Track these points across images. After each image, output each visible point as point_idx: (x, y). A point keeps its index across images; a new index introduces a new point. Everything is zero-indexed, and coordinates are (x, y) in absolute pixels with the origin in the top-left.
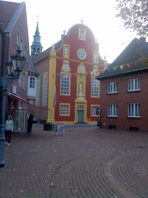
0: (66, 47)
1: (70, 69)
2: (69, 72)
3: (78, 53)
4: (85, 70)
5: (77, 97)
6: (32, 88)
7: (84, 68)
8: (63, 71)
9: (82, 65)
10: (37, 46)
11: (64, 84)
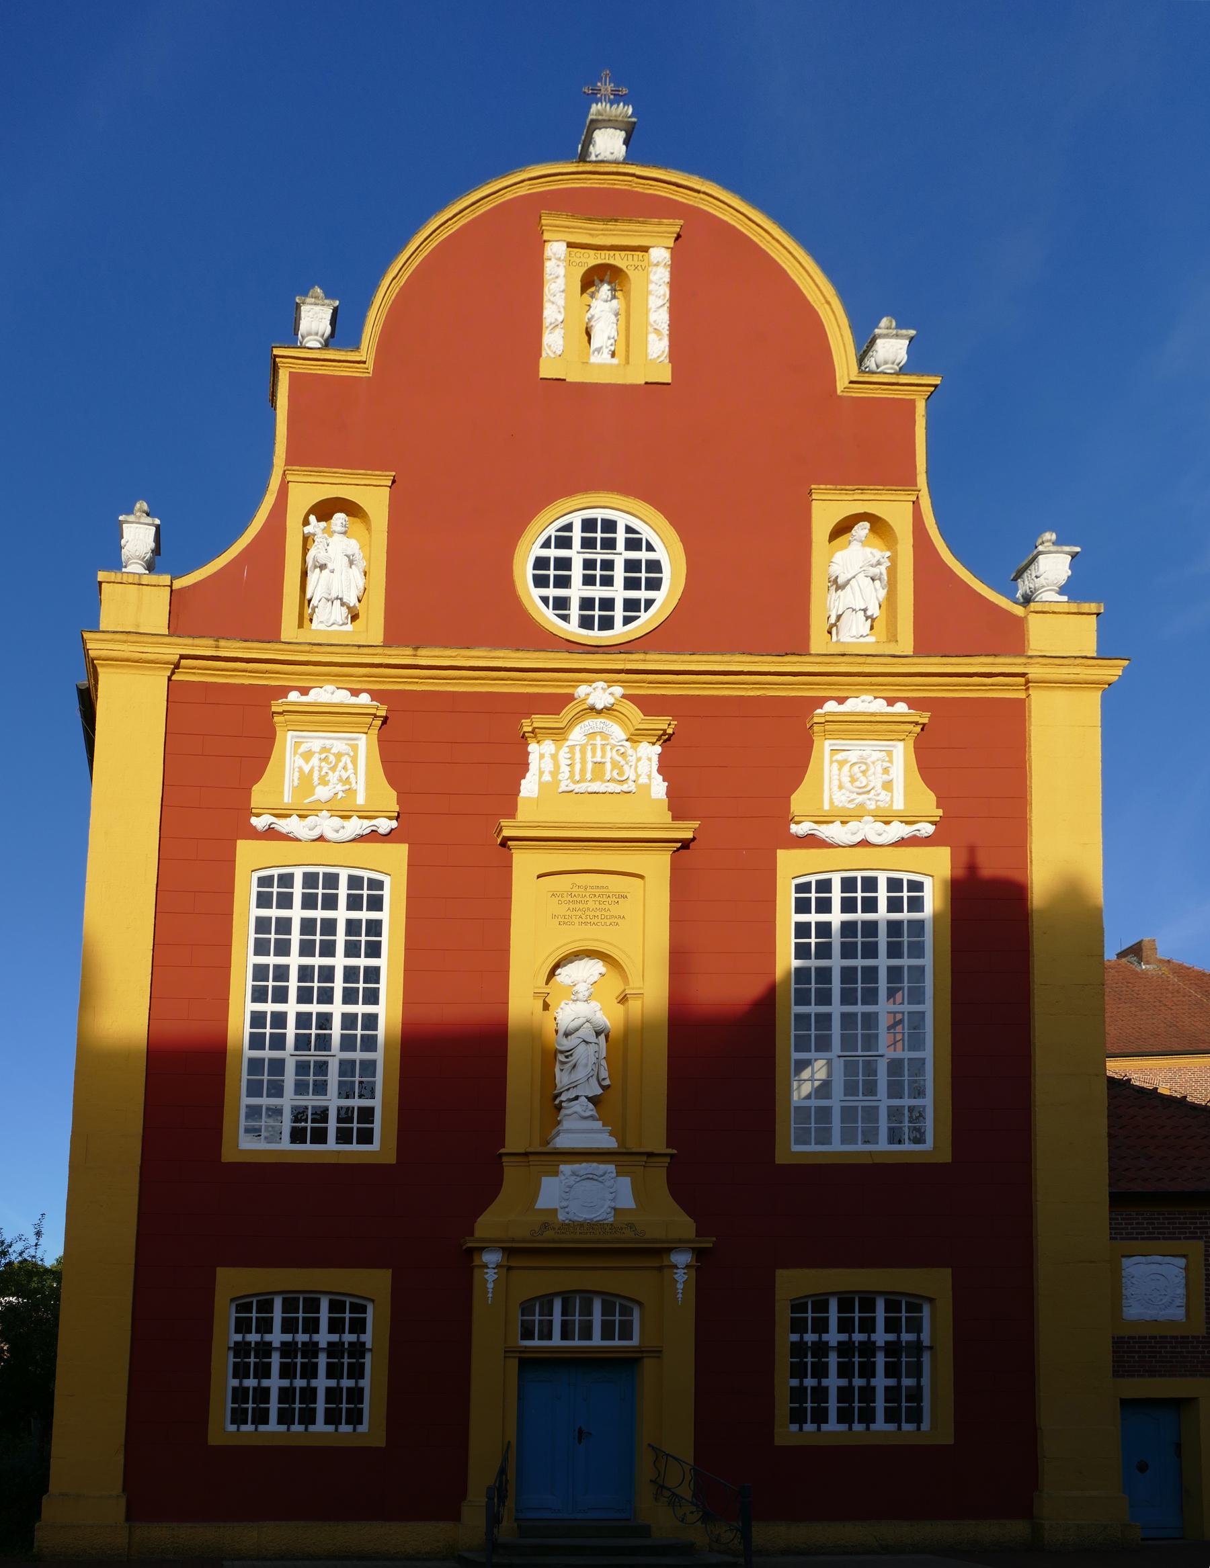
0: (324, 510)
1: (389, 799)
2: (373, 836)
3: (525, 572)
4: (659, 788)
5: (512, 1174)
6: (321, 870)
7: (650, 752)
8: (271, 834)
9: (607, 711)
10: (693, 1255)
11: (322, 1383)
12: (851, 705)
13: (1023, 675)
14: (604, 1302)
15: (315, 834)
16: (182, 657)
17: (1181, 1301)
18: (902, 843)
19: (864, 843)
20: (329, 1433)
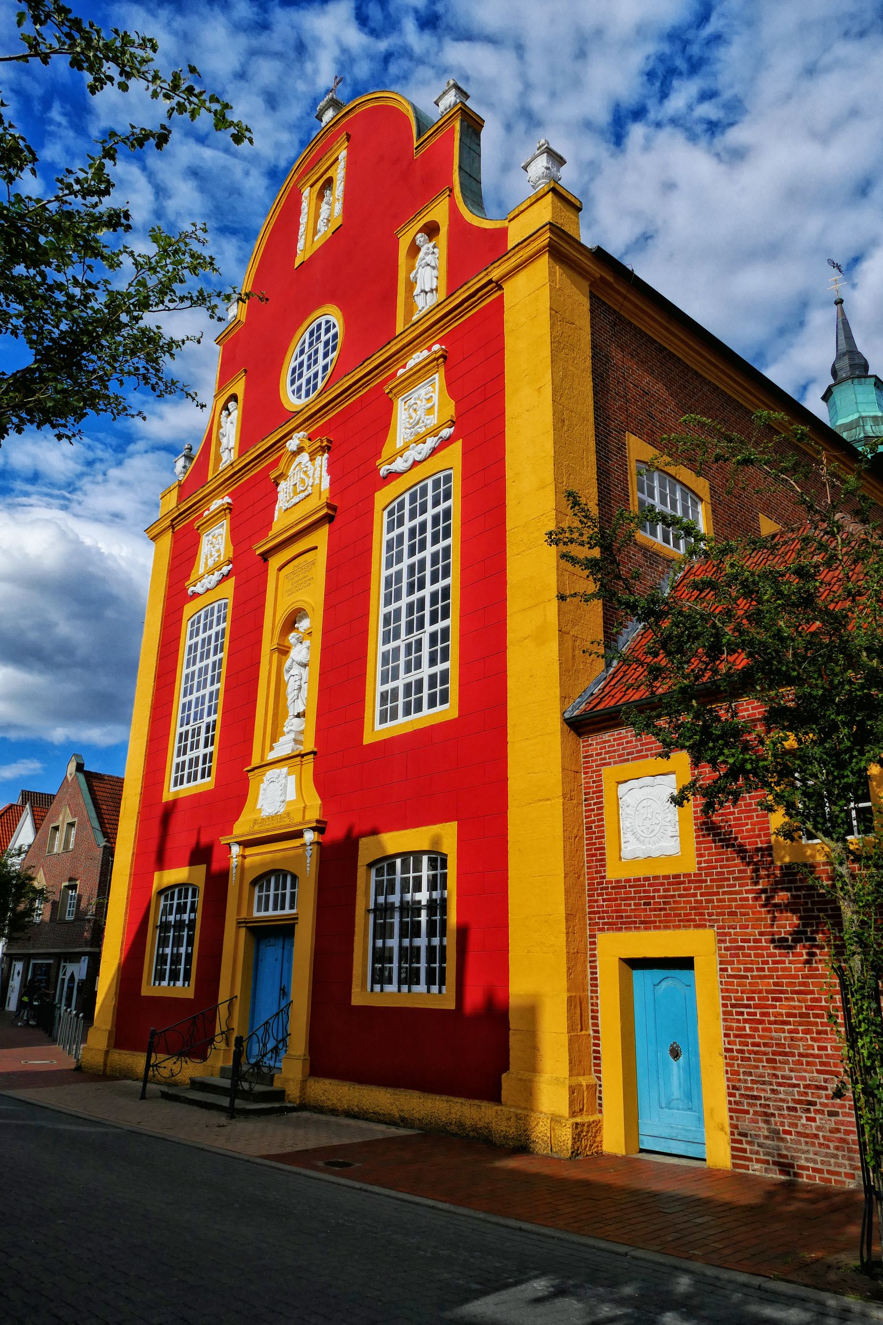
12: (213, 507)
13: (490, 282)
14: (430, 859)
15: (410, 462)
16: (172, 521)
17: (674, 830)
18: (434, 451)
19: (415, 463)
20: (421, 994)
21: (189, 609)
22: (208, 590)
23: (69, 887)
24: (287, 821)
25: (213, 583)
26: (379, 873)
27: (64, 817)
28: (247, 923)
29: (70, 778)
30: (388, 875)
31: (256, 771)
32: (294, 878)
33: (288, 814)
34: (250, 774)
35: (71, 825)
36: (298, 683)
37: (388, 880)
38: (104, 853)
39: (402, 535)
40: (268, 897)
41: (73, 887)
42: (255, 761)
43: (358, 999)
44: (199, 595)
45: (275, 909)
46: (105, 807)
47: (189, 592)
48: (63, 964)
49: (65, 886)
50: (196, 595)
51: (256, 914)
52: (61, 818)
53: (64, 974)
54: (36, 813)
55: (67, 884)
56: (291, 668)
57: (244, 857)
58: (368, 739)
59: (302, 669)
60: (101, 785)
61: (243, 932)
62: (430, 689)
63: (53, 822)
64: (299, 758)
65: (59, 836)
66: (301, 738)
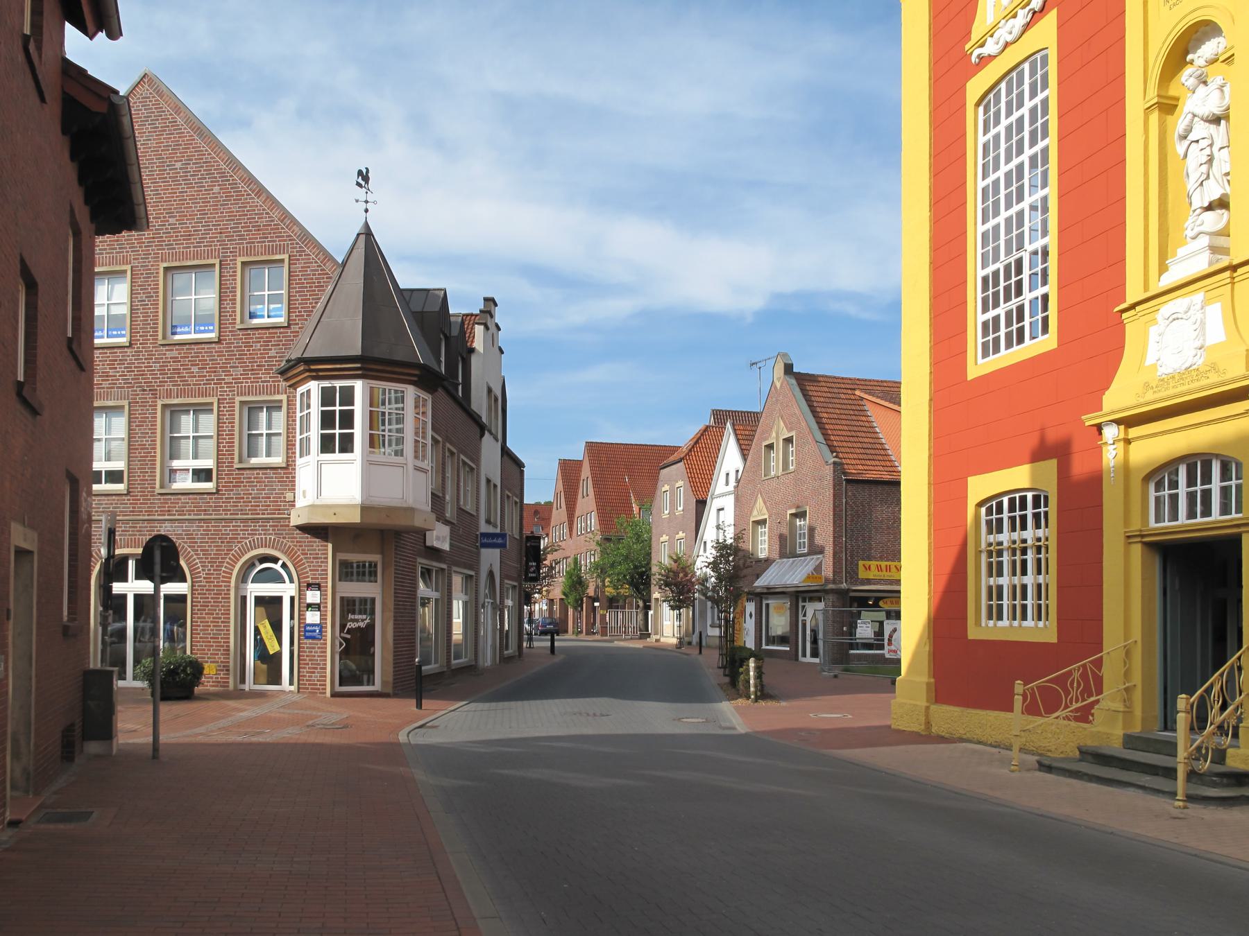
15: (1002, 43)
18: (1027, 27)
21: (975, 87)
22: (1007, 45)
23: (795, 515)
24: (1214, 378)
25: (1016, 31)
26: (1159, 486)
27: (778, 432)
28: (1143, 536)
29: (778, 385)
30: (1020, 510)
31: (1138, 308)
32: (1239, 465)
33: (1214, 367)
34: (1124, 316)
35: (788, 441)
36: (1208, 151)
37: (996, 519)
38: (834, 471)
39: (1021, 119)
40: (1174, 499)
41: (801, 515)
42: (1133, 293)
43: (973, 634)
44: (991, 58)
45: (1191, 514)
46: (825, 415)
47: (974, 59)
48: (801, 604)
49: (792, 515)
50: (985, 60)
51: (1152, 524)
52: (774, 435)
53: (805, 615)
54: (738, 432)
55: (793, 511)
56: (1189, 130)
57: (1128, 442)
58: (970, 377)
59: (1213, 127)
60: (817, 389)
61: (1137, 550)
62: (1006, 328)
63: (766, 439)
64: (1227, 274)
65: (777, 456)
66: (1221, 241)
